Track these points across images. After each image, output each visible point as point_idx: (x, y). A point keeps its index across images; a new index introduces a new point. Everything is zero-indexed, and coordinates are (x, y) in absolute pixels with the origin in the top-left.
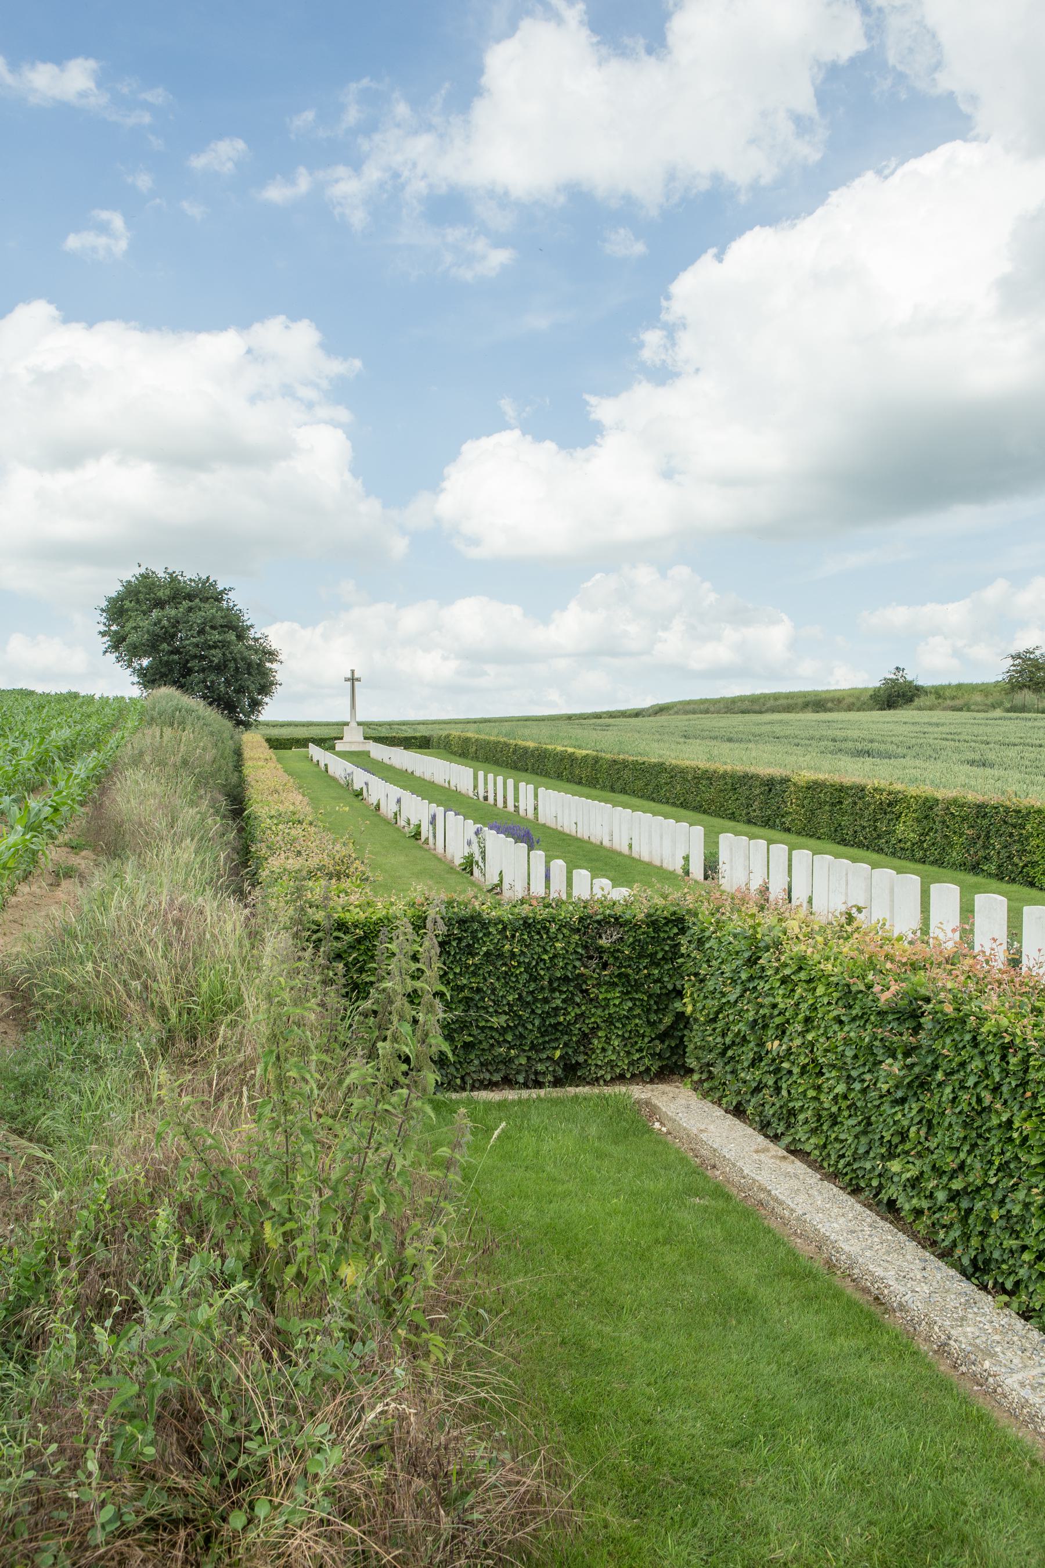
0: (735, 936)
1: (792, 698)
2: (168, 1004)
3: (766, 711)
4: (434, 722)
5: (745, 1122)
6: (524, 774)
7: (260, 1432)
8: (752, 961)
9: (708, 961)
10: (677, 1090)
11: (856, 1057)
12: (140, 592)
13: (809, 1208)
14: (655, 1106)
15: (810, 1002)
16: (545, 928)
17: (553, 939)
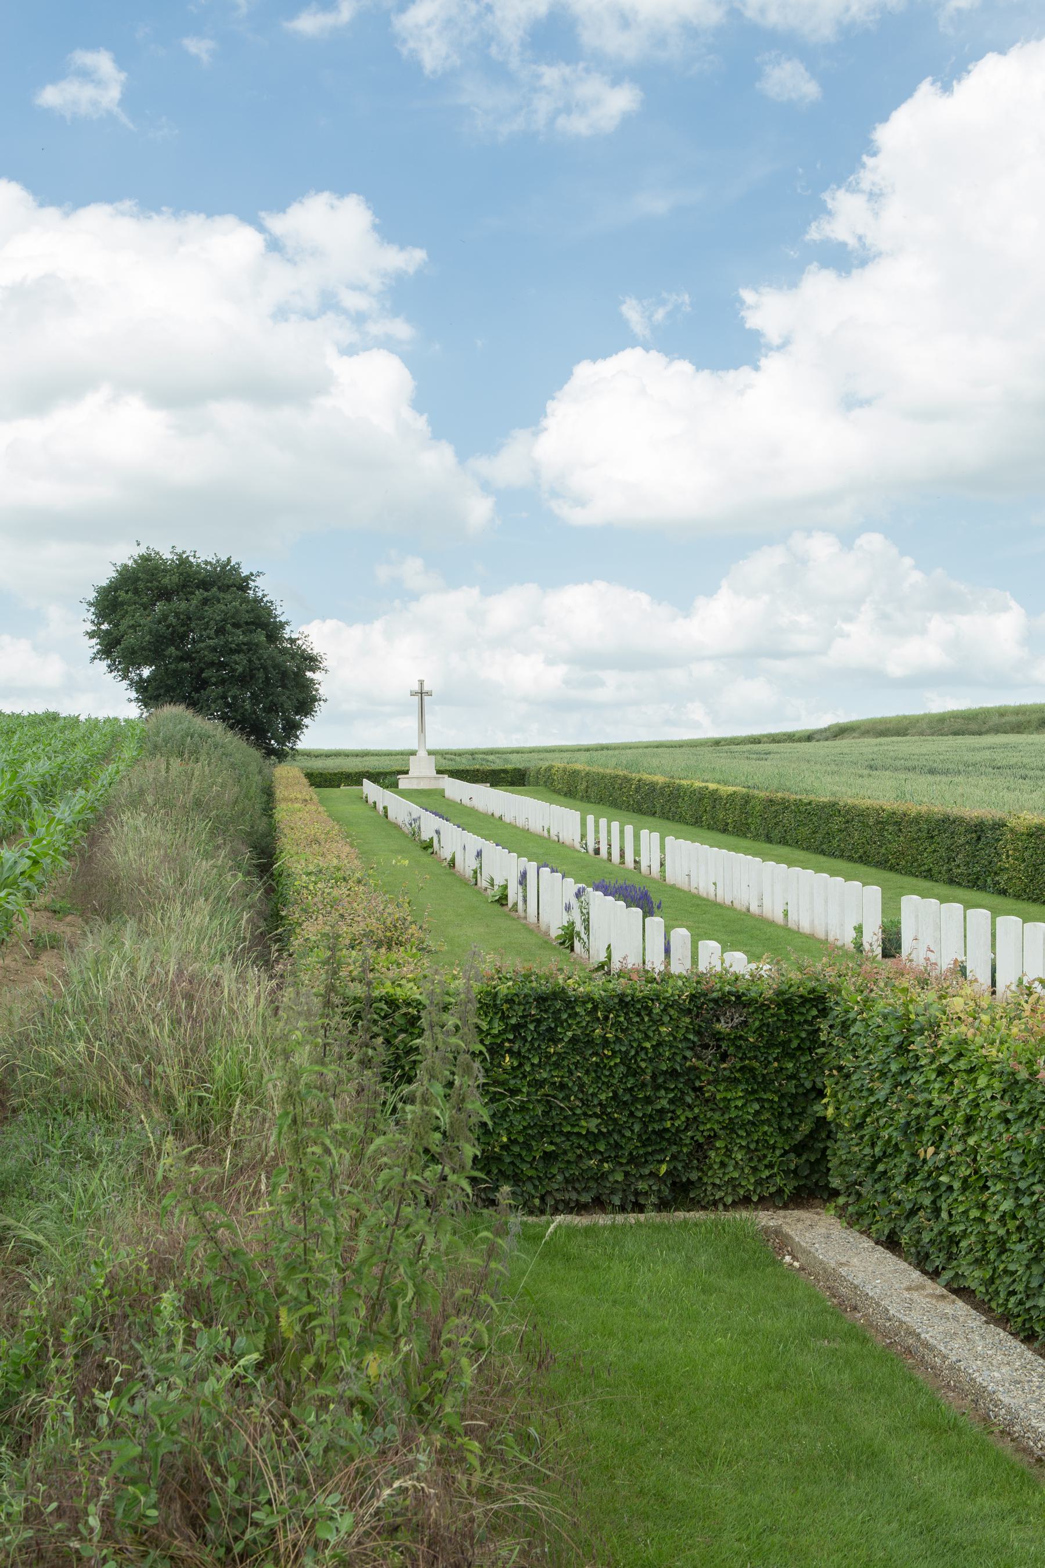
0: (885, 1017)
1: (1024, 713)
2: (175, 1093)
3: (987, 732)
4: (532, 751)
5: (900, 1256)
6: (651, 819)
7: (269, 1502)
8: (902, 1049)
9: (854, 1050)
10: (817, 1217)
11: (1024, 1164)
12: (138, 579)
13: (966, 1354)
14: (787, 1236)
15: (971, 1097)
16: (646, 1008)
17: (658, 1022)
